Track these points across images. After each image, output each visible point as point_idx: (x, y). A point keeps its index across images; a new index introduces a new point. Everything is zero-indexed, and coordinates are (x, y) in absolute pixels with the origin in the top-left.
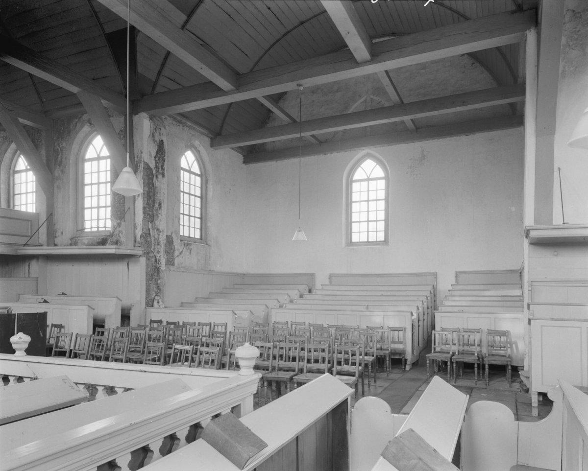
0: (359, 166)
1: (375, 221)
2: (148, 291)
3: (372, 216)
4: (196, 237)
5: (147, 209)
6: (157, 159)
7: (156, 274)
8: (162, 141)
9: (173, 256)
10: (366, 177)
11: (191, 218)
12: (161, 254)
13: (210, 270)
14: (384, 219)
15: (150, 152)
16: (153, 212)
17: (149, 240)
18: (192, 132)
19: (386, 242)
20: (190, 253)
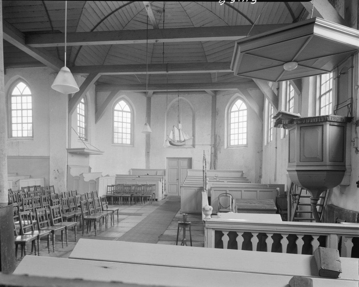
0: (234, 103)
1: (242, 133)
3: (25, 120)
4: (127, 143)
14: (246, 132)
19: (33, 137)
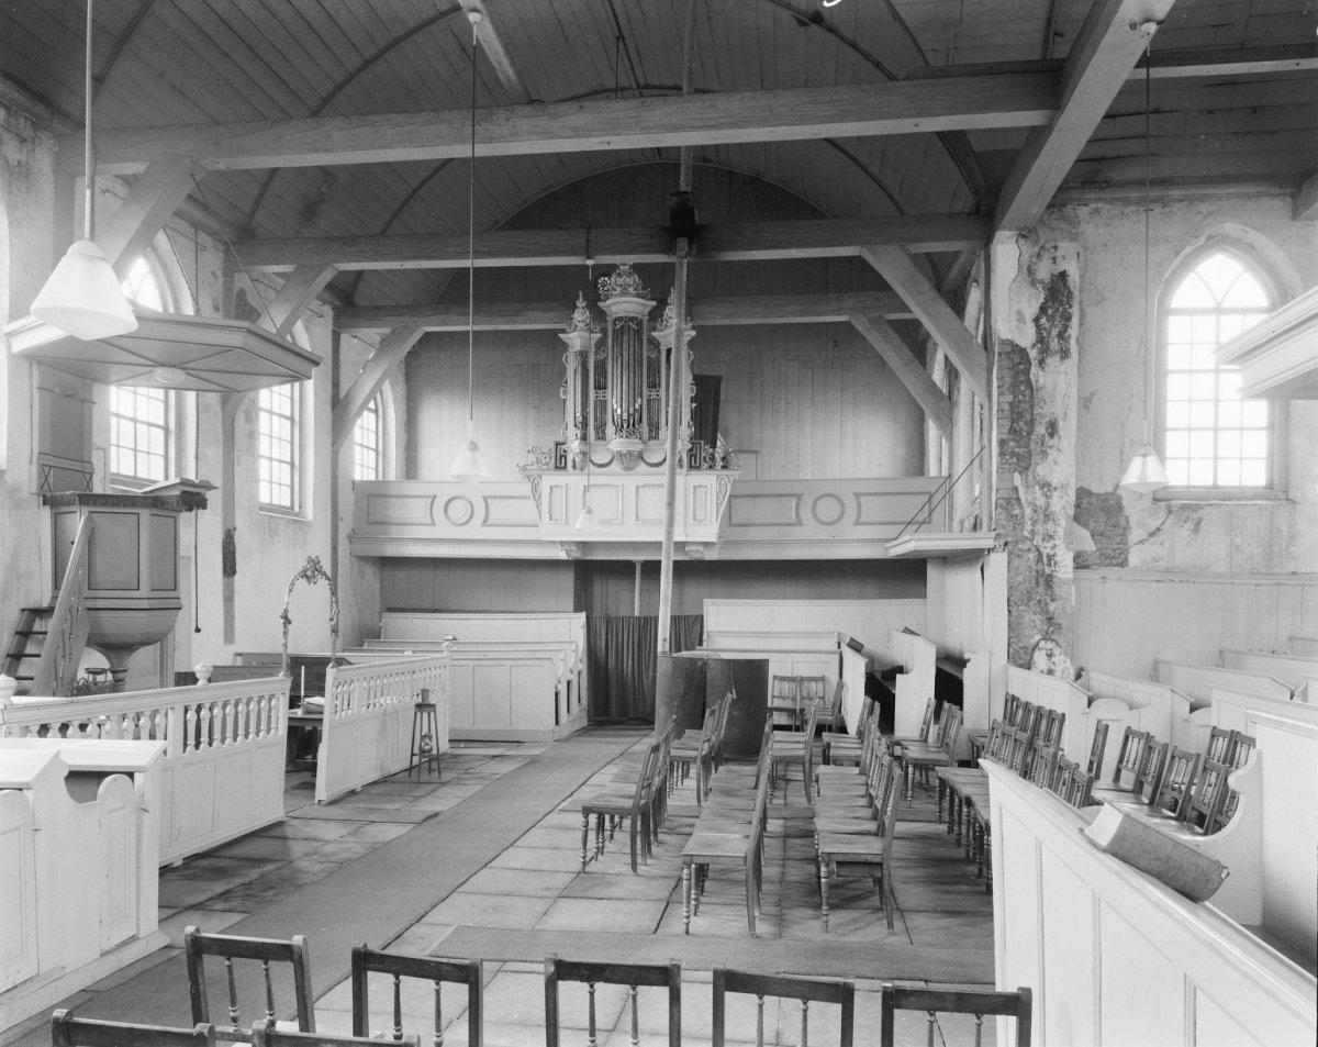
2: (1013, 628)
5: (1012, 444)
6: (1043, 321)
7: (1041, 589)
8: (1063, 275)
9: (1123, 542)
10: (1212, 304)
11: (138, 425)
12: (1057, 542)
13: (1294, 573)
15: (1019, 313)
16: (1027, 447)
17: (1017, 511)
18: (1203, 207)
20: (1196, 530)
